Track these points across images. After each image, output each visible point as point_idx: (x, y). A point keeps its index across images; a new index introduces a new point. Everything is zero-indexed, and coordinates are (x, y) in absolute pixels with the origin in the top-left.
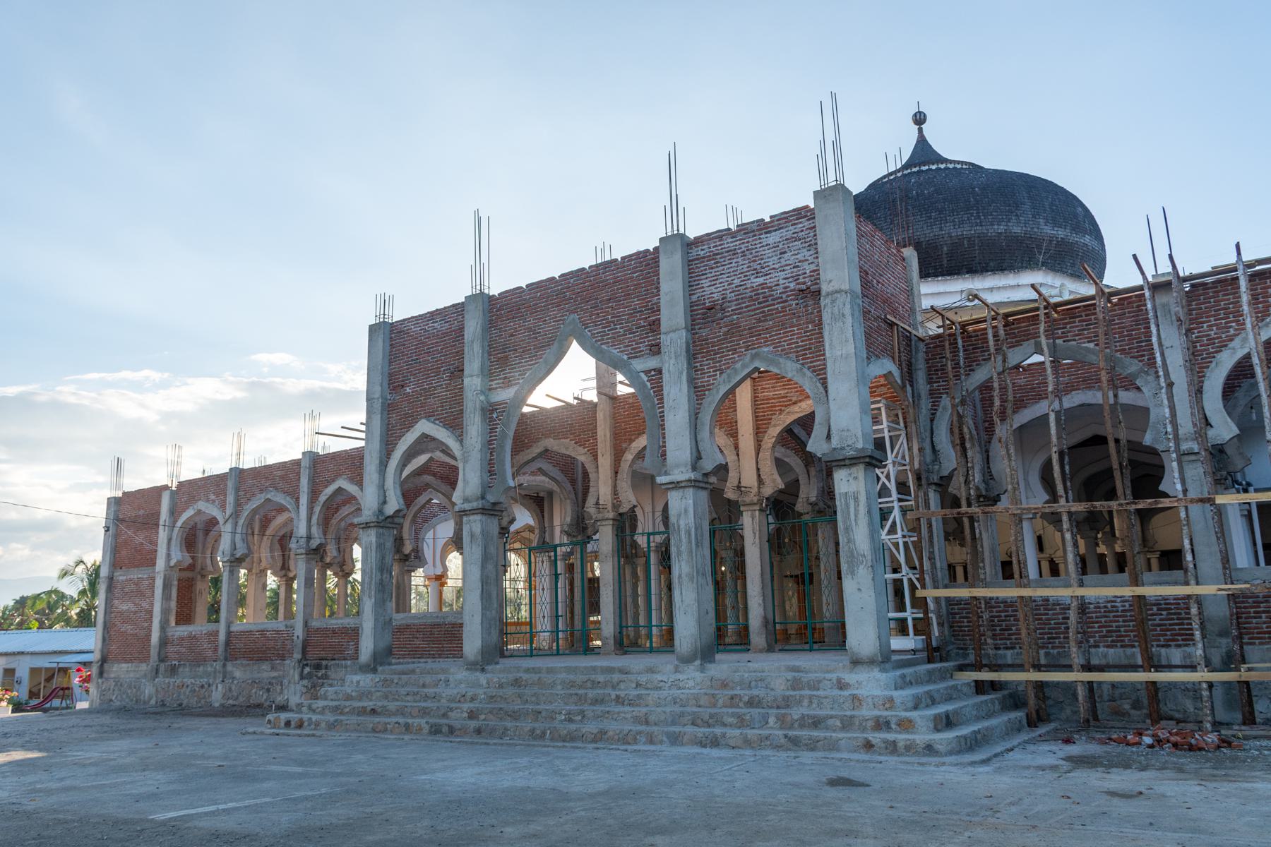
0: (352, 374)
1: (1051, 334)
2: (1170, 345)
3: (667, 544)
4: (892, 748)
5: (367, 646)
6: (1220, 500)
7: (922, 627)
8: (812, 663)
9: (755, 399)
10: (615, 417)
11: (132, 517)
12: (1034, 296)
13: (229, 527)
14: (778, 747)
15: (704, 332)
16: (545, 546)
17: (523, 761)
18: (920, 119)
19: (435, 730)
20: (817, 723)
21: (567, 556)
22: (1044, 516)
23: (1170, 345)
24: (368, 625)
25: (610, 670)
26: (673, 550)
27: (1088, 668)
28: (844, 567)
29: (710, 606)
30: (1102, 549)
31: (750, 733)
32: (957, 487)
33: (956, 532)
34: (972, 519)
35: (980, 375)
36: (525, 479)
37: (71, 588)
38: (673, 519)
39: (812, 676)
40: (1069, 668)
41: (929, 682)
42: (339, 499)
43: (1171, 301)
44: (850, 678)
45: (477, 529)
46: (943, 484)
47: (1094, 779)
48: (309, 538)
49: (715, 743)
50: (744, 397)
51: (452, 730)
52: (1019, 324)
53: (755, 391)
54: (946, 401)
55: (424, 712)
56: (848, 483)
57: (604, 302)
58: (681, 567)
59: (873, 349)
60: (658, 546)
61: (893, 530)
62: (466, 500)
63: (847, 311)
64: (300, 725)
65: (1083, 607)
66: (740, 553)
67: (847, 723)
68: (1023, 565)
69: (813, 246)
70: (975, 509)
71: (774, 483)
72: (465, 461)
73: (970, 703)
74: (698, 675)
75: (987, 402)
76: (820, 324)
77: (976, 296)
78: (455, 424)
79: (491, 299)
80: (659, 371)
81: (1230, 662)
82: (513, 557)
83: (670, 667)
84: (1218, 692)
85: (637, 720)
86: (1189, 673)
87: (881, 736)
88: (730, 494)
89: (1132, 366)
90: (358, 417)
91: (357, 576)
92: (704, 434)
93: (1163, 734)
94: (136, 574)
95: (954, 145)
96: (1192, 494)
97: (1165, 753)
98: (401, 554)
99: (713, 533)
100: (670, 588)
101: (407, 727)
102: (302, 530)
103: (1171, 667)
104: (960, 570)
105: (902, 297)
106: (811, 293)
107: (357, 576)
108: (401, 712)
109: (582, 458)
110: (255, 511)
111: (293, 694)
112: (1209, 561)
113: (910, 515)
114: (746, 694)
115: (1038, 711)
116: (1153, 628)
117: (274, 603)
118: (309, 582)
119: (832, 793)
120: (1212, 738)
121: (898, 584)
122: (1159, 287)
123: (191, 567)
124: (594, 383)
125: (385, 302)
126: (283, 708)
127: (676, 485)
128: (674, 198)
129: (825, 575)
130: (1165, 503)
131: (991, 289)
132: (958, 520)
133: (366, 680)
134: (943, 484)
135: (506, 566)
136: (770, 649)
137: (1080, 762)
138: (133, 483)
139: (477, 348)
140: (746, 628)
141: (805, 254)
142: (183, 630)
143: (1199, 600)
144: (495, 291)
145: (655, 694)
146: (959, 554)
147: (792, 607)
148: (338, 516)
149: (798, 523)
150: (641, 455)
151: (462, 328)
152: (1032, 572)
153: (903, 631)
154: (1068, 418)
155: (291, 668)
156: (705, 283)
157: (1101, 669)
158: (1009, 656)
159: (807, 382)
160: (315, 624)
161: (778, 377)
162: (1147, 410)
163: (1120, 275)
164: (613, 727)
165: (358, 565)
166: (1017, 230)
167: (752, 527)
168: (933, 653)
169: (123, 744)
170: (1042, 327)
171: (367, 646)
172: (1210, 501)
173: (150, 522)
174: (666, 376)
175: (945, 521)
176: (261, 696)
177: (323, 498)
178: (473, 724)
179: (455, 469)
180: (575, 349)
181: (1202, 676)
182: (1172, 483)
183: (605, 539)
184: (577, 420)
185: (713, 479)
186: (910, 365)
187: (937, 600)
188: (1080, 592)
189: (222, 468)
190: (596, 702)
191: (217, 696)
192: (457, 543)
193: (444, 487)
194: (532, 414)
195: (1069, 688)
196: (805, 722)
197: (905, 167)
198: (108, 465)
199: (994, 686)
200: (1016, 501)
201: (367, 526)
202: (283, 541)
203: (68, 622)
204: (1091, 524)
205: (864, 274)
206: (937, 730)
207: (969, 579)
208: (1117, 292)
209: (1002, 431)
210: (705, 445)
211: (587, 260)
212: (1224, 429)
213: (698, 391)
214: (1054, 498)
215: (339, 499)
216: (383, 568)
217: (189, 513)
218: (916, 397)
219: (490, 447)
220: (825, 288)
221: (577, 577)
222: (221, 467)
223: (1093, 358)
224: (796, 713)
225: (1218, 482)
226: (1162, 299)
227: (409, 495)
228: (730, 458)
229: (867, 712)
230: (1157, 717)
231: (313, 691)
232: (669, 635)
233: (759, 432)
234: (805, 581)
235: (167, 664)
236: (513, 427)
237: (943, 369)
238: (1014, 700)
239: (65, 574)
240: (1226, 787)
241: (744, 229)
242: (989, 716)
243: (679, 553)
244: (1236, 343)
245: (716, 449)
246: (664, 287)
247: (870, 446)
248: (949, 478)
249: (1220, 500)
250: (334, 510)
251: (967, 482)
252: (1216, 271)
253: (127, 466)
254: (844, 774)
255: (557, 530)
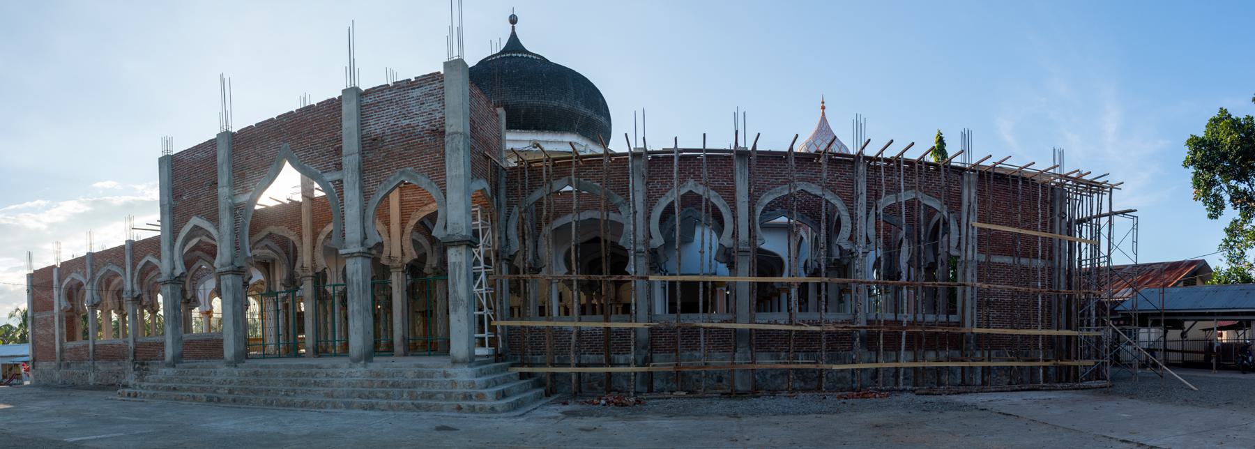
0: (150, 191)
1: (577, 174)
2: (637, 187)
3: (345, 291)
4: (472, 409)
5: (169, 353)
6: (651, 278)
7: (493, 342)
8: (430, 363)
9: (401, 201)
10: (313, 212)
11: (40, 282)
12: (570, 149)
13: (89, 287)
14: (409, 410)
15: (370, 156)
16: (271, 293)
17: (261, 417)
18: (513, 20)
19: (210, 400)
20: (431, 396)
21: (284, 299)
22: (564, 281)
23: (637, 187)
24: (169, 341)
25: (311, 366)
26: (349, 295)
27: (579, 365)
28: (451, 307)
29: (371, 329)
30: (595, 301)
31: (392, 402)
32: (518, 262)
33: (516, 288)
34: (525, 281)
35: (536, 195)
36: (258, 252)
37: (15, 323)
38: (349, 276)
39: (429, 370)
40: (569, 365)
41: (495, 373)
42: (148, 267)
43: (640, 163)
44: (451, 371)
45: (229, 283)
46: (510, 260)
47: (575, 423)
48: (133, 291)
49: (372, 408)
50: (394, 199)
51: (219, 400)
52: (562, 165)
53: (401, 196)
54: (516, 209)
55: (203, 390)
56: (456, 257)
57: (303, 134)
58: (353, 306)
59: (475, 173)
60: (340, 293)
61: (480, 286)
62: (222, 266)
63: (461, 146)
64: (135, 396)
65: (580, 332)
66: (390, 298)
67: (448, 396)
68: (550, 308)
69: (441, 100)
70: (527, 275)
71: (411, 255)
72: (221, 241)
73: (515, 385)
74: (363, 370)
75: (539, 212)
76: (444, 154)
77: (538, 145)
78: (214, 218)
79: (233, 134)
80: (341, 181)
81: (646, 362)
82: (251, 300)
83: (346, 365)
84: (639, 377)
85: (327, 395)
86: (627, 368)
87: (467, 402)
88: (384, 261)
89: (618, 199)
90: (155, 216)
91: (161, 312)
92: (369, 223)
93: (610, 399)
94: (46, 315)
95: (531, 44)
96: (639, 274)
97: (610, 408)
98: (185, 300)
99: (373, 286)
100: (346, 318)
101: (194, 398)
102: (128, 287)
103: (619, 365)
104: (516, 311)
105: (495, 140)
106: (439, 133)
107: (161, 312)
108: (190, 389)
109: (292, 238)
110: (102, 277)
111: (131, 378)
112: (642, 312)
113: (491, 278)
114: (390, 380)
115: (551, 388)
116: (611, 344)
117: (117, 329)
118: (134, 316)
119: (438, 434)
120: (633, 400)
121: (481, 317)
122: (637, 155)
123: (72, 310)
124: (299, 189)
125: (167, 142)
126: (126, 386)
127: (351, 255)
128: (352, 62)
129: (439, 311)
130: (626, 278)
131: (547, 142)
132: (517, 281)
133: (170, 372)
134: (510, 260)
135: (247, 305)
136: (405, 355)
137: (568, 414)
138: (39, 265)
139: (225, 168)
140: (392, 342)
141: (436, 105)
142: (71, 344)
143: (635, 330)
144: (235, 129)
145: (337, 380)
146: (517, 301)
147: (419, 330)
148: (148, 278)
149: (425, 280)
150: (329, 236)
151: (215, 156)
152: (555, 313)
153: (482, 344)
154: (582, 225)
155: (128, 365)
156: (372, 122)
157: (585, 366)
158: (539, 359)
159: (434, 192)
160: (140, 340)
161: (416, 188)
162: (622, 225)
163: (617, 145)
164: (312, 399)
165: (161, 306)
166: (565, 106)
167: (397, 282)
168: (498, 357)
169: (47, 403)
170: (573, 169)
171: (169, 353)
172: (646, 278)
173: (49, 286)
174: (345, 184)
175: (510, 282)
176: (114, 380)
177: (139, 267)
178: (231, 397)
179: (215, 247)
180: (287, 167)
181: (633, 369)
182: (630, 268)
183: (307, 288)
184: (289, 213)
185: (374, 252)
186: (497, 185)
187: (502, 327)
188: (579, 324)
189: (82, 253)
190: (302, 384)
191: (91, 379)
192: (218, 292)
193: (209, 258)
194: (261, 210)
195: (568, 375)
196: (423, 396)
197: (502, 52)
198: (25, 256)
199: (530, 375)
200: (550, 272)
201: (165, 283)
202: (119, 293)
203: (15, 340)
204: (589, 287)
205: (472, 122)
206: (497, 399)
207: (521, 316)
208: (615, 155)
209: (546, 230)
210: (370, 230)
211: (294, 106)
212: (658, 241)
213: (365, 195)
214: (570, 272)
215: (148, 267)
216: (176, 308)
217: (67, 280)
218: (499, 205)
219: (236, 232)
220: (448, 130)
221: (291, 312)
222: (82, 253)
223: (598, 192)
224: (419, 391)
225: (651, 269)
226: (637, 162)
227: (188, 264)
228: (385, 238)
229: (459, 390)
230: (609, 390)
231: (141, 377)
232: (346, 346)
233: (403, 222)
234: (428, 315)
235: (64, 363)
236: (249, 219)
237: (516, 189)
238: (539, 382)
239: (11, 316)
240: (634, 423)
241: (399, 86)
242: (526, 391)
243: (352, 298)
244: (668, 194)
245: (376, 232)
246: (345, 124)
247: (470, 234)
248: (515, 256)
249: (651, 278)
250: (146, 274)
251: (524, 259)
252: (665, 151)
253: (34, 256)
254: (445, 424)
255: (278, 283)
